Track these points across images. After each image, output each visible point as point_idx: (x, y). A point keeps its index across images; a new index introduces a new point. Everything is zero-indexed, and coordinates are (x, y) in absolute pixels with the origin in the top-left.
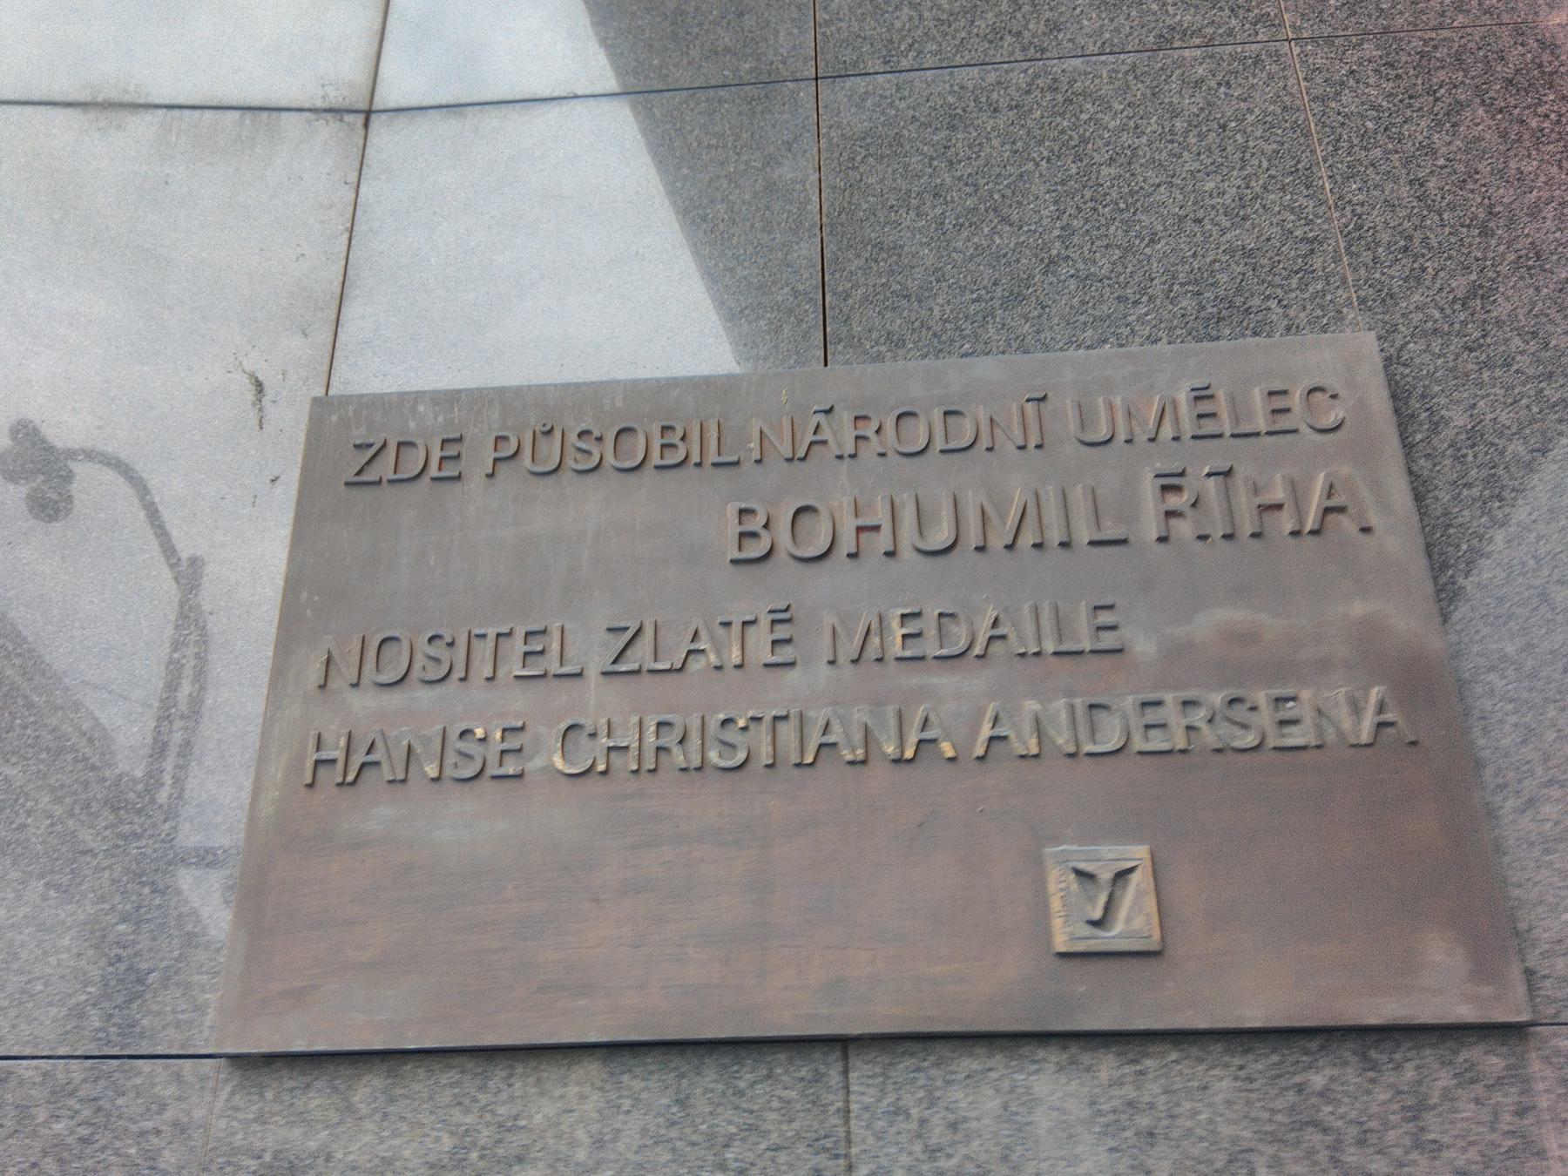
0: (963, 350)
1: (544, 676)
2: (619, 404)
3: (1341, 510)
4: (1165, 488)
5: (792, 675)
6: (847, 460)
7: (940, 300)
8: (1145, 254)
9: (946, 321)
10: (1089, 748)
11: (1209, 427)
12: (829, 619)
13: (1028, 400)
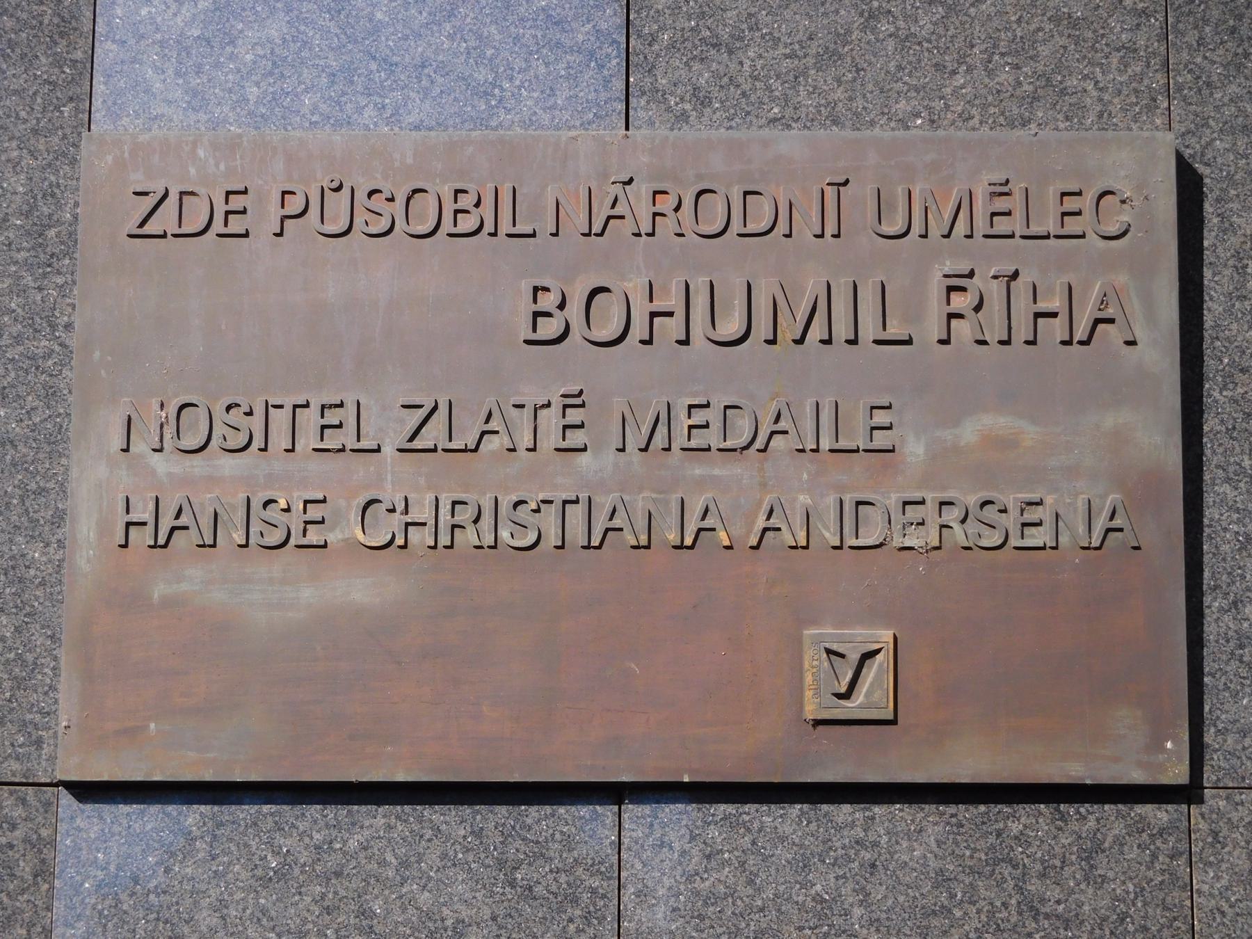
0: (771, 115)
1: (342, 450)
2: (410, 161)
3: (1111, 321)
4: (951, 289)
5: (583, 459)
6: (644, 237)
7: (751, 54)
8: (969, 16)
9: (756, 78)
10: (854, 542)
11: (1002, 225)
12: (618, 405)
13: (828, 184)
